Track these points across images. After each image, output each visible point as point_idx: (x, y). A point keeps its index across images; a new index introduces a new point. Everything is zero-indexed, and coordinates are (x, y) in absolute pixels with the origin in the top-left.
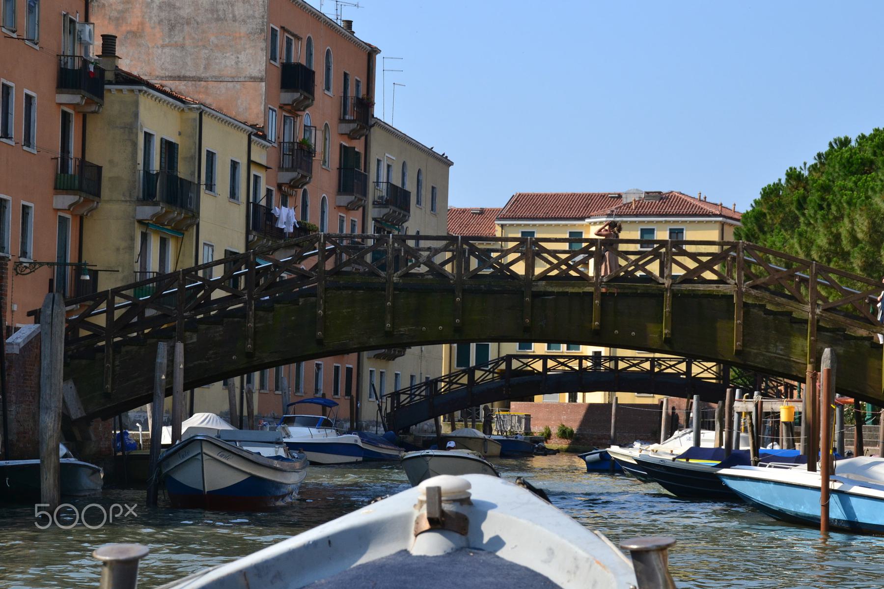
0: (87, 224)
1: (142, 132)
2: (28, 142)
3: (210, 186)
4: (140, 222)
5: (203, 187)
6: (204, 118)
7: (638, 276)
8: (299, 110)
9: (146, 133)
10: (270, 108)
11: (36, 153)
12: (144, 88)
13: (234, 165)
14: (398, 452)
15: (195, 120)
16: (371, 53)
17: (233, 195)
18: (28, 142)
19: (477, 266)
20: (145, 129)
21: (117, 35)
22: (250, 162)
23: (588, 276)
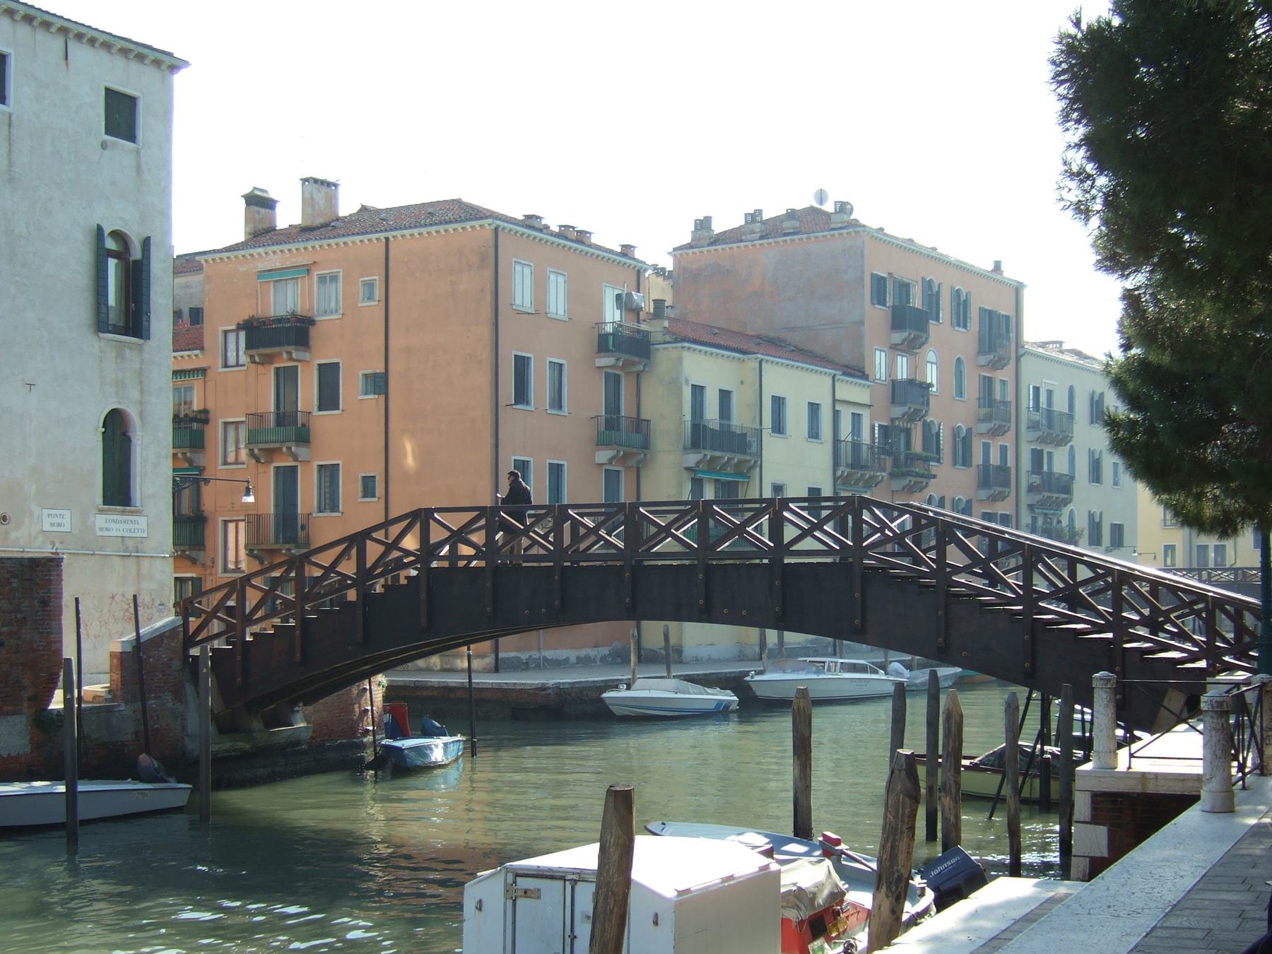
0: (643, 473)
1: (688, 384)
2: (557, 403)
3: (778, 428)
4: (688, 469)
5: (767, 433)
6: (764, 365)
7: (382, 590)
8: (915, 348)
9: (694, 386)
10: (876, 349)
11: (567, 414)
12: (687, 345)
13: (814, 408)
14: (85, 811)
15: (755, 368)
16: (1018, 289)
17: (814, 433)
18: (557, 403)
19: (569, 543)
20: (691, 382)
21: (665, 299)
22: (834, 401)
23: (228, 600)
